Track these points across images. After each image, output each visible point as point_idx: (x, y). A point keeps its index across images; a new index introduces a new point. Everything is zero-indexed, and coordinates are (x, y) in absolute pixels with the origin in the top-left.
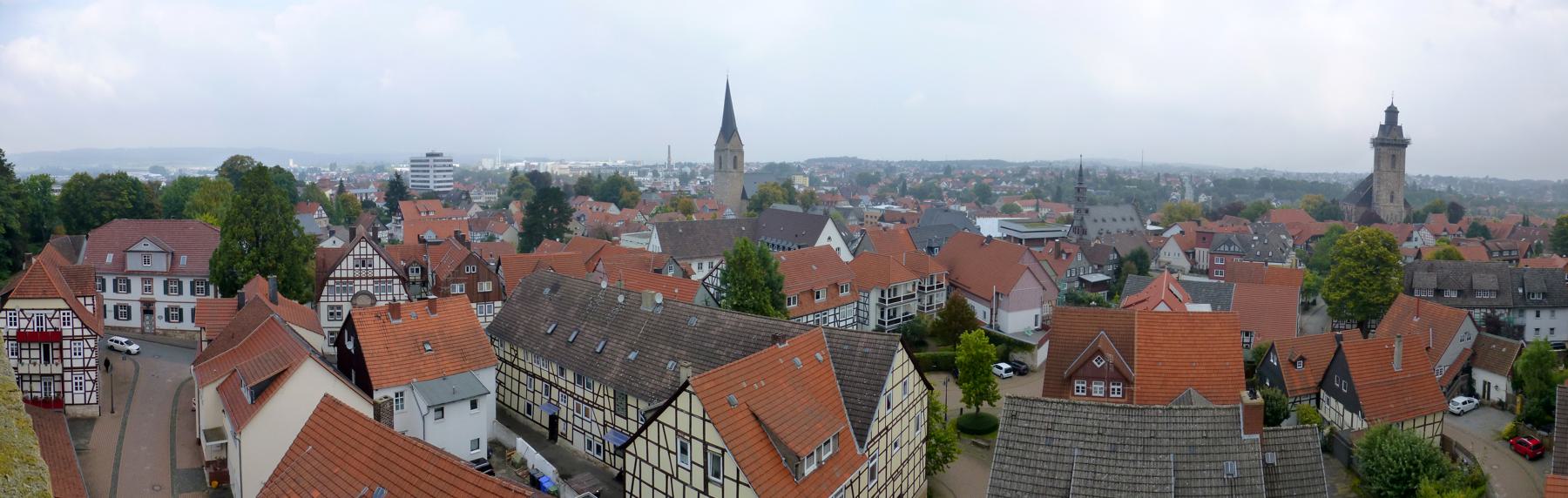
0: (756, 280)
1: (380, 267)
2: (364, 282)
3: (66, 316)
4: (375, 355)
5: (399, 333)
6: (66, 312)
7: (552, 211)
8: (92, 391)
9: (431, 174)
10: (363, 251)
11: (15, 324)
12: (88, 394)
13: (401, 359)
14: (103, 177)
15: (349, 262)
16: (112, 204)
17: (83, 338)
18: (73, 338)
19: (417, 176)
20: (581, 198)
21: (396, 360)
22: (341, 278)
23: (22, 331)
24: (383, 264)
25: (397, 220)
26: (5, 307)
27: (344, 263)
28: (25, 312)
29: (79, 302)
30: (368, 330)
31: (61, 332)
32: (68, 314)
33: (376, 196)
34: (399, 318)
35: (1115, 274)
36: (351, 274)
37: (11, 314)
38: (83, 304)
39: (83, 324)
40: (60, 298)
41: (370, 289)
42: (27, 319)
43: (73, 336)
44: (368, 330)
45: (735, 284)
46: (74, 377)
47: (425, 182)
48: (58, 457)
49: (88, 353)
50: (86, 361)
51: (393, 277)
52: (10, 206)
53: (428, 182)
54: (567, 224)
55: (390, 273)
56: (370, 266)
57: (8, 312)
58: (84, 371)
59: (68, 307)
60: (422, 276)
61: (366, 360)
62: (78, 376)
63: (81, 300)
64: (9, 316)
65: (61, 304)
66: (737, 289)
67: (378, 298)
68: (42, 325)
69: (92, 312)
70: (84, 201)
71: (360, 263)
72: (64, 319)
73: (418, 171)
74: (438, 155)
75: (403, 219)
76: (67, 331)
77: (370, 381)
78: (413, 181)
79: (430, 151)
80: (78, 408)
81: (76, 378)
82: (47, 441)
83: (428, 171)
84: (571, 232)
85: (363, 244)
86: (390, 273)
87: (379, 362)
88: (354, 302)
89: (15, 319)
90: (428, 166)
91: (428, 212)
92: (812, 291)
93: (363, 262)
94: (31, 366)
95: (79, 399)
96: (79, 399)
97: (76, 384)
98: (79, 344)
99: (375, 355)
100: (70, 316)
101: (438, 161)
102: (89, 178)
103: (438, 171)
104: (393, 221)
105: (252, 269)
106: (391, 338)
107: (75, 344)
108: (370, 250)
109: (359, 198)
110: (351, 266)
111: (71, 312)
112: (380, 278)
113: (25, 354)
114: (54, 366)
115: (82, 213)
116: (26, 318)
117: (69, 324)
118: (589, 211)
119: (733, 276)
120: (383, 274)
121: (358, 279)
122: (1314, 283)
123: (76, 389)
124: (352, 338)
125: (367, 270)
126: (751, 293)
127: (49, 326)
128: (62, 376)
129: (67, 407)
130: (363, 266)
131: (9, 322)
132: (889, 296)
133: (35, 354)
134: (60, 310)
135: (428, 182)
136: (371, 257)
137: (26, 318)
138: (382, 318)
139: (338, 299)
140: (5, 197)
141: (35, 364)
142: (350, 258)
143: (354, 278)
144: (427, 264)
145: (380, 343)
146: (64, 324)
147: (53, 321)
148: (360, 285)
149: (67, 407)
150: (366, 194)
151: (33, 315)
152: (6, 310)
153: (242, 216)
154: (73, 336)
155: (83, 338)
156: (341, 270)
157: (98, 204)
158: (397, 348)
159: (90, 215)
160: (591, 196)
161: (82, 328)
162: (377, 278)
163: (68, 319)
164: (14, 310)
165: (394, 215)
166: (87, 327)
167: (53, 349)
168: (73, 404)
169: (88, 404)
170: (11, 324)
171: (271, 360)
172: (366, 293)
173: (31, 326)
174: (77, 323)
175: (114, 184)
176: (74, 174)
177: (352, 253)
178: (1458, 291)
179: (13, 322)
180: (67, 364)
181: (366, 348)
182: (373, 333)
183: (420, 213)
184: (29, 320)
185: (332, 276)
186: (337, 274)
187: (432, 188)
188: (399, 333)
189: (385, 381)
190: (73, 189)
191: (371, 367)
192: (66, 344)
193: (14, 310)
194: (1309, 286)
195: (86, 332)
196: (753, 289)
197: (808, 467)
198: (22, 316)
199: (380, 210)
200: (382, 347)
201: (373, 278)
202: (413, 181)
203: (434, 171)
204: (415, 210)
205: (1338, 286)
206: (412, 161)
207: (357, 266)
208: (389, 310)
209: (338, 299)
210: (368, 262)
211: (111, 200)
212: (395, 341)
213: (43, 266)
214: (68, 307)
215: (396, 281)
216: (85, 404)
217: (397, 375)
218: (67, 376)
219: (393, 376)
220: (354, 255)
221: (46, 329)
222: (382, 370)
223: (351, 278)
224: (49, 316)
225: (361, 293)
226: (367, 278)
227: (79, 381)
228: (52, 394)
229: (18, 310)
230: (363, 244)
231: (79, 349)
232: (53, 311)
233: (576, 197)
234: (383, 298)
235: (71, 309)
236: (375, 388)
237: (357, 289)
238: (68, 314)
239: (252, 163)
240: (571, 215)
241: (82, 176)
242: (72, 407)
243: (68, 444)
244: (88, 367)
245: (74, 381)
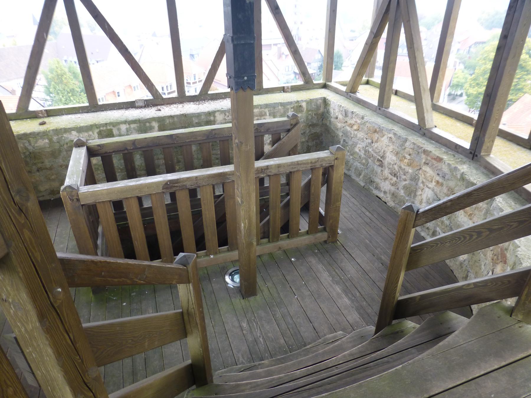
0: (73, 89)
35: (319, 69)
45: (58, 94)
48: (501, 203)
66: (61, 97)
92: (114, 92)
119: (55, 88)
122: (463, 81)
126: (72, 98)
132: (167, 90)
171: (44, 352)
178: (272, 134)
194: (458, 82)
196: (73, 95)
197: (424, 239)
205: (478, 84)
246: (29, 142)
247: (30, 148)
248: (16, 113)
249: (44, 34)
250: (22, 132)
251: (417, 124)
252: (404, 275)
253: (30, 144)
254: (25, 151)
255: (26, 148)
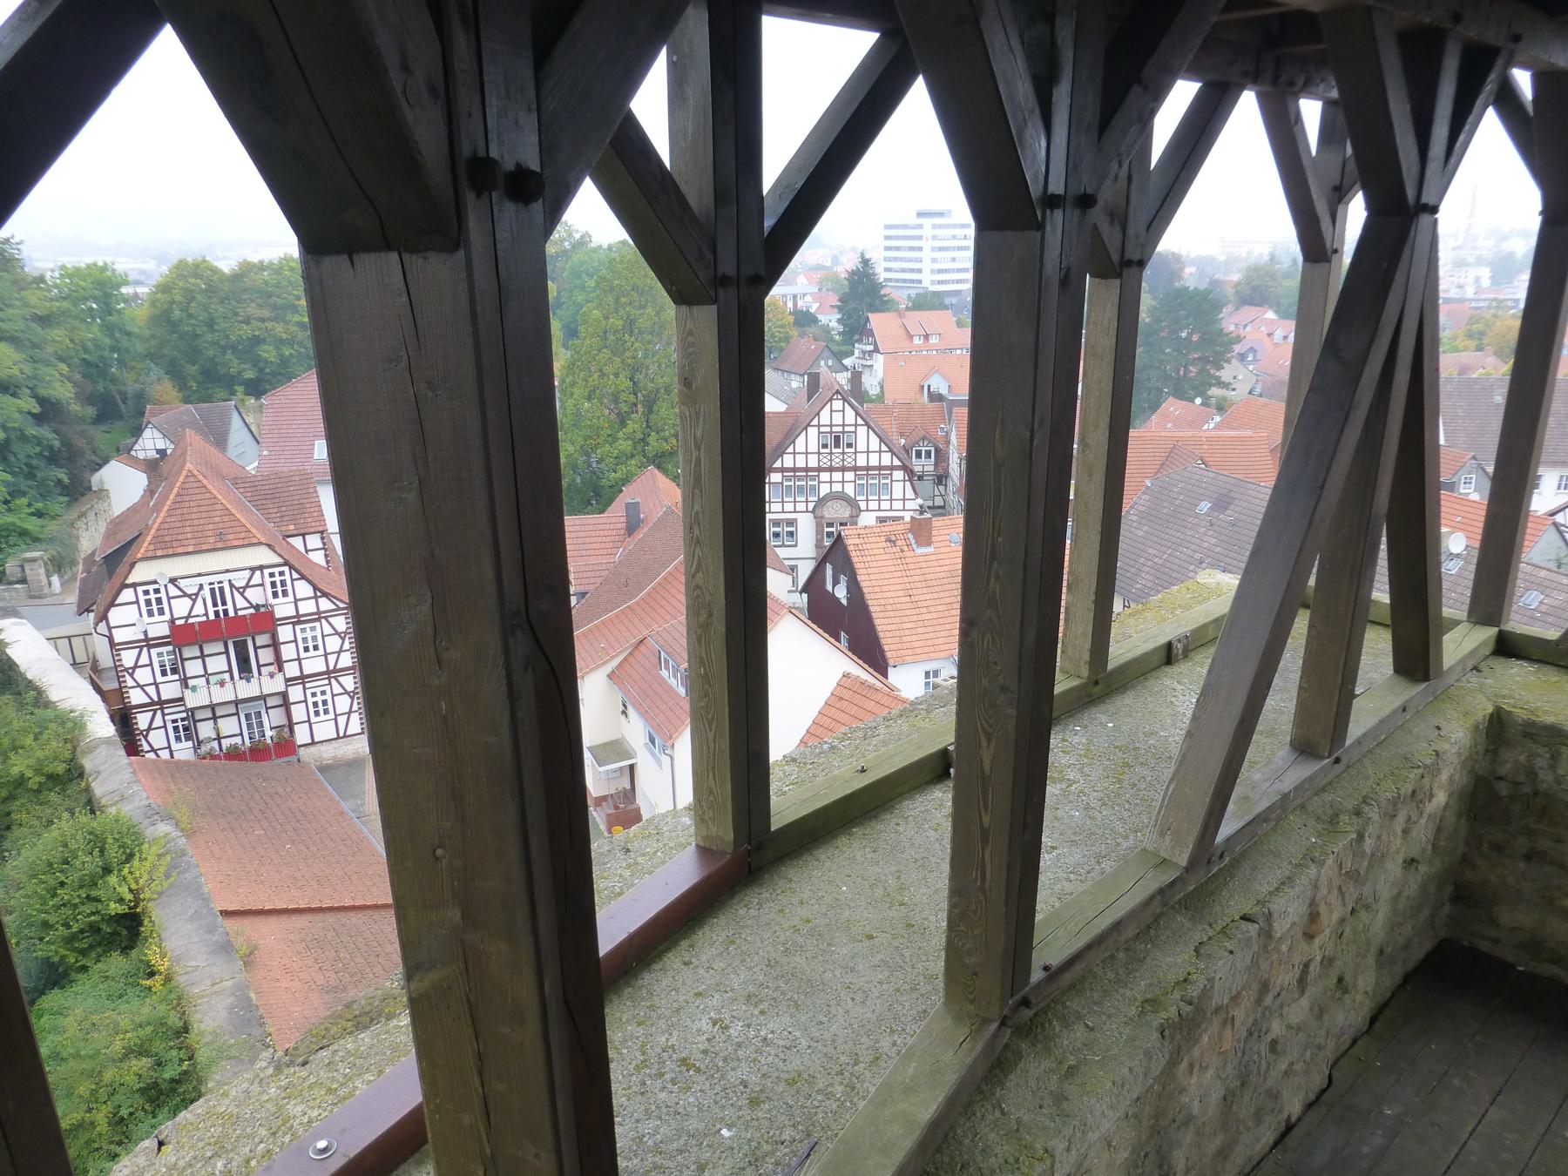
1: (868, 447)
2: (837, 476)
3: (278, 579)
4: (889, 608)
5: (930, 570)
6: (276, 570)
7: (1188, 339)
8: (349, 713)
9: (926, 255)
10: (837, 419)
11: (161, 612)
12: (342, 720)
13: (935, 615)
14: (247, 269)
15: (808, 441)
16: (279, 329)
17: (319, 616)
18: (298, 620)
19: (895, 259)
20: (1249, 312)
21: (926, 617)
22: (794, 470)
23: (181, 622)
24: (875, 443)
25: (864, 352)
26: (130, 580)
27: (800, 442)
28: (182, 583)
29: (293, 547)
30: (875, 564)
31: (271, 614)
32: (281, 574)
33: (815, 300)
34: (929, 544)
36: (813, 462)
37: (146, 593)
38: (303, 551)
39: (315, 588)
40: (260, 543)
41: (850, 490)
42: (189, 596)
43: (298, 615)
44: (875, 564)
46: (309, 692)
47: (912, 271)
49: (333, 643)
50: (332, 659)
51: (892, 468)
52: (35, 346)
53: (920, 271)
54: (1220, 368)
55: (887, 459)
56: (849, 445)
57: (140, 589)
58: (329, 679)
59: (280, 560)
60: (936, 465)
61: (874, 615)
62: (318, 691)
63: (297, 542)
64: (142, 599)
65: (264, 556)
67: (863, 505)
68: (224, 603)
69: (324, 564)
70: (210, 324)
71: (830, 440)
72: (273, 584)
73: (898, 249)
74: (941, 214)
75: (876, 350)
76: (283, 608)
77: (882, 652)
78: (887, 270)
79: (922, 208)
80: (323, 748)
81: (314, 695)
82: (300, 816)
83: (920, 249)
84: (1226, 386)
85: (837, 404)
86: (887, 459)
87: (898, 620)
88: (818, 513)
89: (159, 601)
90: (920, 238)
91: (926, 337)
93: (837, 439)
94: (215, 689)
95: (324, 730)
96: (324, 730)
97: (315, 704)
98: (313, 629)
99: (889, 608)
100: (287, 577)
101: (941, 226)
102: (215, 270)
103: (941, 249)
104: (857, 353)
105: (633, 456)
106: (917, 578)
107: (303, 630)
108: (850, 416)
109: (790, 304)
110: (813, 447)
111: (286, 569)
112: (868, 468)
113: (193, 668)
114: (265, 679)
115: (211, 353)
116: (185, 595)
117: (285, 593)
118: (1266, 340)
120: (874, 461)
121: (825, 470)
123: (317, 713)
124: (843, 578)
125: (843, 453)
127: (241, 603)
128: (284, 695)
129: (302, 752)
130: (838, 445)
131: (144, 609)
133: (217, 664)
134: (261, 568)
135: (920, 271)
136: (853, 429)
137: (185, 595)
138: (899, 543)
139: (789, 507)
140: (21, 325)
141: (222, 684)
142: (813, 432)
143: (819, 469)
144: (948, 442)
145: (898, 587)
146: (275, 595)
147: (248, 593)
148: (831, 482)
149: (302, 752)
150: (795, 297)
151: (201, 587)
152: (134, 585)
153: (606, 354)
154: (298, 615)
155: (319, 616)
156: (794, 453)
157: (246, 331)
158: (926, 597)
159: (229, 355)
160: (1271, 307)
161: (316, 597)
162: (861, 469)
163: (283, 583)
164: (155, 582)
165: (860, 341)
166: (325, 595)
167: (256, 648)
168: (313, 743)
169: (345, 736)
170: (150, 613)
172: (841, 497)
173: (199, 609)
174: (303, 589)
175: (277, 286)
176: (175, 262)
177: (815, 422)
179: (155, 606)
180: (292, 670)
181: (873, 596)
182: (884, 570)
183: (911, 337)
184: (193, 598)
185: (778, 464)
186: (788, 461)
187: (926, 283)
188: (930, 570)
189: (910, 652)
190: (178, 298)
191: (884, 628)
192: (285, 633)
193: (155, 582)
195: (325, 604)
198: (173, 591)
199: (827, 330)
200: (901, 593)
201: (855, 469)
202: (887, 270)
203: (933, 249)
204: (902, 331)
206: (888, 227)
207: (825, 446)
208: (911, 530)
209: (789, 507)
210: (845, 440)
211: (276, 319)
212: (924, 584)
213: (205, 482)
214: (279, 560)
215: (898, 475)
216: (339, 738)
217: (930, 643)
218: (295, 693)
219: (923, 643)
220: (819, 426)
221: (236, 610)
222: (902, 633)
223: (813, 469)
224: (238, 584)
225: (833, 496)
226: (843, 469)
227: (319, 698)
228: (269, 733)
229: (163, 581)
230: (837, 404)
231: (315, 638)
232: (247, 574)
233: (1237, 309)
234: (873, 505)
235: (286, 563)
236: (891, 662)
237: (824, 490)
238: (281, 574)
239: (570, 235)
240: (1230, 350)
241: (196, 266)
242: (313, 749)
243: (342, 813)
244: (335, 670)
245: (310, 700)
246: (1553, 758)
247: (1545, 777)
248: (1557, 642)
249: (1317, 152)
250: (1550, 719)
251: (776, 823)
252: (38, 628)
253: (1553, 767)
254: (1522, 778)
255: (1531, 773)
